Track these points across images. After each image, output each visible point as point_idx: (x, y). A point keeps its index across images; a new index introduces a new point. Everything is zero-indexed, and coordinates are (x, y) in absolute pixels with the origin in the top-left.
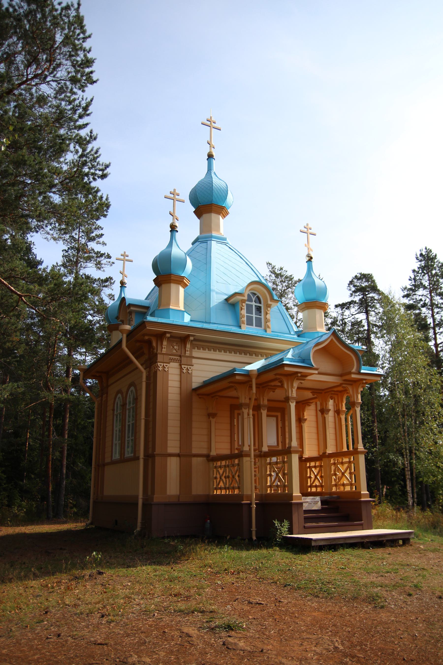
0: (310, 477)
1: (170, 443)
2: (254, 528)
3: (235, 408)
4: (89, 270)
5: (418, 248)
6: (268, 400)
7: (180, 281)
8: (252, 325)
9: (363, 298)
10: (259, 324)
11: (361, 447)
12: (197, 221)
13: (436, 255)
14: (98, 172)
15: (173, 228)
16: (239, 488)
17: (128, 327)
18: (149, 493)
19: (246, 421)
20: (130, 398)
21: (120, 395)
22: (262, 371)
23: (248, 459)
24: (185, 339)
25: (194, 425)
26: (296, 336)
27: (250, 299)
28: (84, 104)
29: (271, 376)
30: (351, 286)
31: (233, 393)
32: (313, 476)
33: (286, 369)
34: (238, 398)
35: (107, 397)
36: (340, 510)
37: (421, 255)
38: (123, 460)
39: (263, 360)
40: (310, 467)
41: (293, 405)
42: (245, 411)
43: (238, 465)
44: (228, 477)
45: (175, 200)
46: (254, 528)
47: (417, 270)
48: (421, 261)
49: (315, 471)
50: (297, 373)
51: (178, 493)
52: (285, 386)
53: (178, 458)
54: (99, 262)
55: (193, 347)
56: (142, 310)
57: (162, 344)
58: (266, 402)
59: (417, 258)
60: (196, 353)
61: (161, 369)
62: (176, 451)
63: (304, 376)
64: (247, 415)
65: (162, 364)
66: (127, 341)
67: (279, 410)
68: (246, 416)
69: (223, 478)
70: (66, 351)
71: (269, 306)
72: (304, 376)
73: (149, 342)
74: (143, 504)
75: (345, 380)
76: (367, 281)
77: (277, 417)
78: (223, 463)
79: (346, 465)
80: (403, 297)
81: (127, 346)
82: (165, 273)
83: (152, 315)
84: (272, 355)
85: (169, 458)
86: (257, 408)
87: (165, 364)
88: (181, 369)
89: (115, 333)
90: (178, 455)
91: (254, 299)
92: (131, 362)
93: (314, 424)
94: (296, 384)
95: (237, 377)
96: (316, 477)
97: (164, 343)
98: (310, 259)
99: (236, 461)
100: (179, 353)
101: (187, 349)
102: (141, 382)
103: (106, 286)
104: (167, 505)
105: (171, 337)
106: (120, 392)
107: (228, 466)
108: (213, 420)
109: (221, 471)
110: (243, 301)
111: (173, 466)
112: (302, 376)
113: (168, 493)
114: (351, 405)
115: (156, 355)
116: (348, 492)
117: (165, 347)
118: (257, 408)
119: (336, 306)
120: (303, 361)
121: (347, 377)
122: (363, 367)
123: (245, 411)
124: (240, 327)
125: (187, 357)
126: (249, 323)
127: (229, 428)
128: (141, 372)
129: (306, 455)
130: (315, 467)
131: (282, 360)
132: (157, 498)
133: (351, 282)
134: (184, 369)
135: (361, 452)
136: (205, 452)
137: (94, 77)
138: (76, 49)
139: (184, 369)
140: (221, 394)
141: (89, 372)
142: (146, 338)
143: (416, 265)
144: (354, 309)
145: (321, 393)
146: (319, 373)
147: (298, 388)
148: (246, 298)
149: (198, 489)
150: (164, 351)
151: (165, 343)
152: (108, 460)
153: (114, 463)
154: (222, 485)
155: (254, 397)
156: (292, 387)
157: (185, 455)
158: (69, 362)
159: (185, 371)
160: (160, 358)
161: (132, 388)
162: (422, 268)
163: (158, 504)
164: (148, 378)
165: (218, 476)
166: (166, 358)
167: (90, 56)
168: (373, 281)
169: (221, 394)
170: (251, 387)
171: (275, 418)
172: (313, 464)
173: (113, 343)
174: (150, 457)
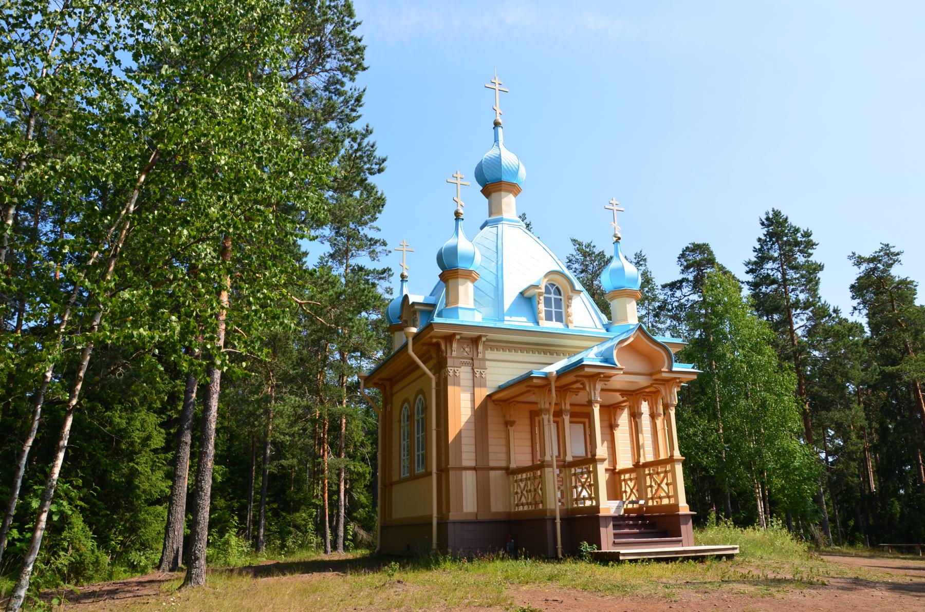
0: (626, 492)
1: (464, 456)
2: (559, 545)
3: (534, 415)
4: (362, 259)
5: (762, 211)
6: (571, 405)
7: (469, 275)
8: (551, 320)
9: (698, 274)
10: (559, 319)
11: (677, 454)
12: (485, 201)
13: (787, 219)
14: (374, 166)
16: (542, 502)
17: (414, 330)
18: (444, 512)
19: (546, 428)
20: (418, 406)
21: (406, 405)
22: (562, 373)
23: (550, 469)
24: (475, 339)
25: (490, 434)
26: (604, 331)
27: (548, 291)
28: (356, 94)
29: (571, 378)
30: (683, 260)
31: (532, 398)
32: (628, 490)
33: (587, 369)
34: (537, 403)
35: (391, 408)
36: (655, 523)
37: (768, 219)
38: (413, 477)
39: (566, 360)
40: (624, 480)
41: (596, 410)
42: (546, 417)
43: (540, 476)
44: (530, 491)
46: (559, 545)
47: (763, 238)
48: (768, 226)
49: (631, 484)
50: (599, 374)
51: (476, 511)
52: (588, 388)
54: (374, 251)
55: (486, 347)
56: (429, 309)
57: (451, 347)
58: (568, 407)
59: (763, 224)
60: (490, 354)
61: (451, 374)
62: (472, 463)
63: (609, 377)
64: (548, 419)
66: (413, 345)
67: (583, 416)
68: (546, 422)
69: (525, 492)
70: (338, 356)
71: (570, 298)
72: (609, 377)
73: (438, 345)
74: (438, 523)
75: (656, 380)
76: (702, 252)
77: (584, 424)
78: (524, 476)
79: (662, 475)
80: (747, 273)
81: (413, 351)
82: (450, 270)
83: (440, 315)
84: (575, 354)
85: (464, 472)
86: (558, 414)
88: (474, 372)
89: (397, 334)
90: (475, 469)
92: (418, 367)
93: (627, 428)
94: (599, 386)
95: (535, 381)
96: (632, 491)
99: (539, 473)
100: (471, 356)
102: (431, 389)
103: (382, 278)
104: (463, 523)
105: (461, 338)
106: (406, 400)
107: (529, 479)
108: (511, 429)
109: (522, 485)
110: (540, 294)
111: (469, 480)
112: (605, 377)
114: (666, 407)
115: (446, 359)
116: (666, 506)
118: (558, 414)
119: (664, 287)
120: (606, 361)
121: (657, 377)
122: (675, 364)
123: (546, 417)
124: (538, 323)
125: (480, 360)
126: (549, 317)
127: (529, 437)
128: (430, 379)
129: (619, 467)
130: (631, 480)
131: (581, 360)
132: (453, 516)
133: (683, 256)
135: (678, 460)
136: (504, 464)
137: (365, 64)
138: (346, 40)
140: (518, 399)
141: (369, 380)
142: (434, 340)
143: (761, 232)
144: (686, 290)
145: (633, 395)
146: (624, 373)
147: (602, 390)
148: (543, 290)
149: (498, 506)
150: (454, 354)
151: (455, 346)
152: (395, 478)
153: (402, 481)
154: (524, 500)
155: (554, 401)
156: (671, 393)
157: (481, 469)
158: (341, 370)
159: (478, 375)
160: (450, 362)
161: (420, 396)
162: (769, 235)
163: (454, 523)
164: (438, 384)
165: (519, 491)
166: (457, 362)
167: (360, 44)
168: (711, 253)
169: (518, 399)
170: (550, 390)
171: (582, 425)
172: (627, 476)
173: (397, 346)
174: (443, 471)
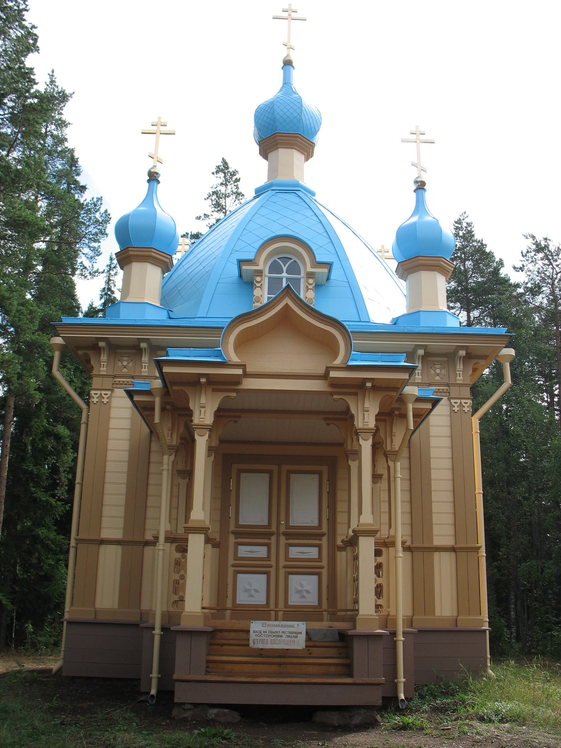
2: (402, 679)
15: (153, 177)
45: (418, 141)
51: (455, 614)
53: (453, 554)
65: (458, 401)
87: (103, 392)
90: (453, 549)
91: (285, 269)
97: (458, 367)
98: (420, 186)
101: (458, 373)
111: (110, 560)
113: (99, 604)
117: (461, 373)
134: (456, 405)
139: (456, 405)
166: (108, 382)
171: (267, 476)
